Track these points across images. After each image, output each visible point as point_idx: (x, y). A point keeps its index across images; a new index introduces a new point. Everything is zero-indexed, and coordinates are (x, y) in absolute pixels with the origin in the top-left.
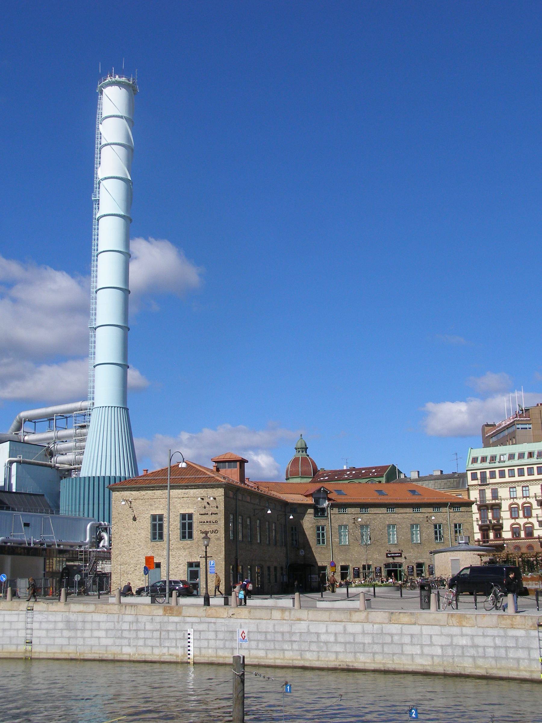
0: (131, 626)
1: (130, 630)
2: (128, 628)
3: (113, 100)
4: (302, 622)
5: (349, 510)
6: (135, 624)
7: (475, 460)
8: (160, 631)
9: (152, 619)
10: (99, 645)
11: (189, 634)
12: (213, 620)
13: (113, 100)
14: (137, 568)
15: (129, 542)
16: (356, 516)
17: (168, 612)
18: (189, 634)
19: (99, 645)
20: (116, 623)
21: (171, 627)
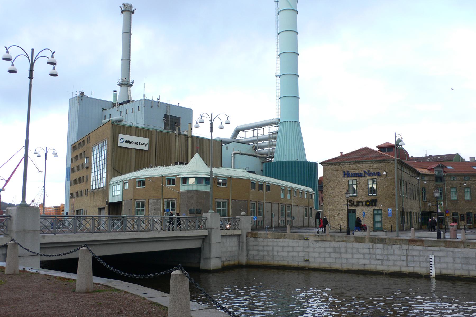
1: (382, 255)
11: (431, 259)
18: (431, 259)
20: (371, 250)
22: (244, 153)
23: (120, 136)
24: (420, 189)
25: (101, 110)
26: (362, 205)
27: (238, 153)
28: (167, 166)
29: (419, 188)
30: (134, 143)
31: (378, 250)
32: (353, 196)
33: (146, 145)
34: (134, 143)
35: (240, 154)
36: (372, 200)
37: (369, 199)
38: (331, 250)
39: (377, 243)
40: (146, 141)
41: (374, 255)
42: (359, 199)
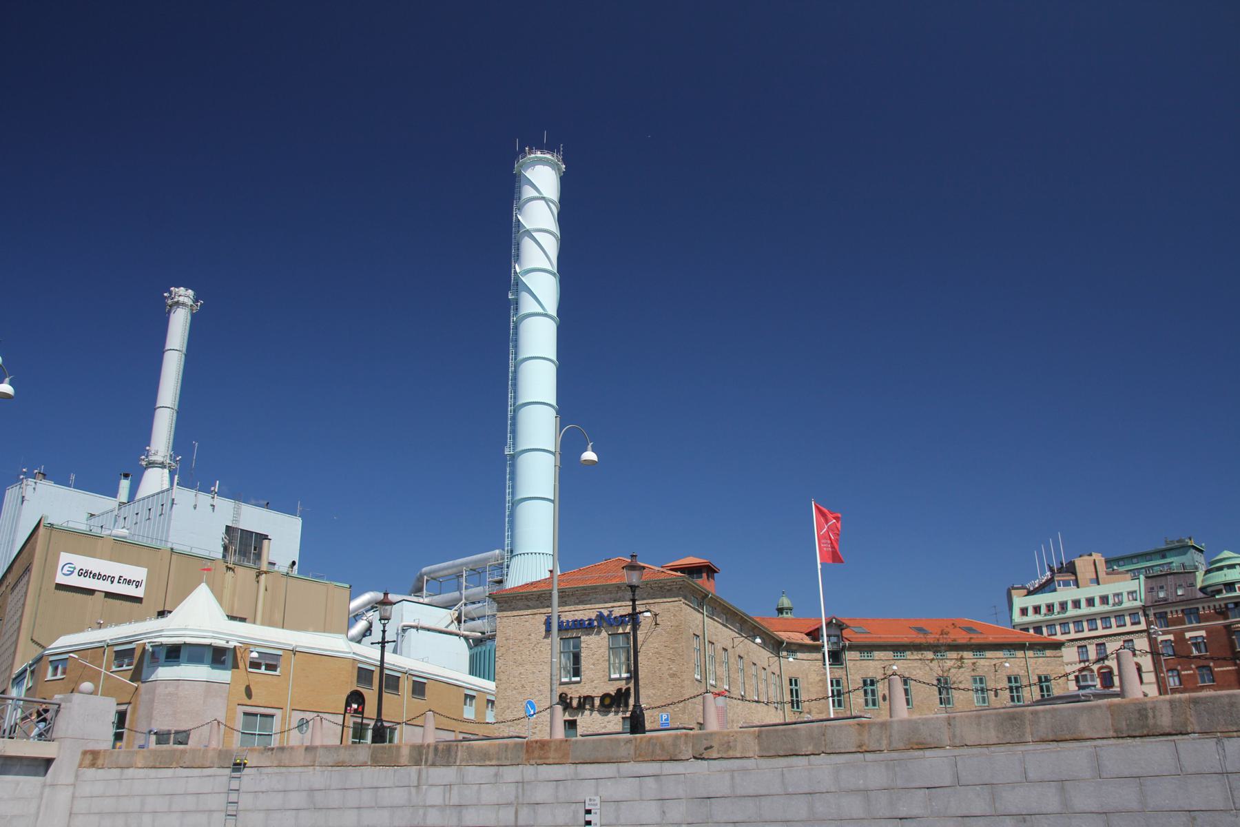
0: (447, 796)
1: (443, 808)
2: (439, 801)
3: (542, 179)
4: (928, 753)
5: (877, 654)
6: (455, 790)
7: (1024, 611)
8: (517, 805)
9: (496, 775)
10: (74, 785)
11: (588, 812)
12: (653, 768)
13: (542, 179)
14: (536, 731)
15: (523, 686)
16: (887, 663)
17: (536, 754)
18: (588, 812)
19: (74, 785)
20: (413, 790)
21: (542, 793)
22: (426, 625)
23: (65, 557)
24: (786, 683)
25: (86, 516)
26: (592, 709)
27: (412, 627)
28: (136, 621)
29: (780, 676)
30: (105, 578)
31: (434, 789)
32: (570, 683)
33: (138, 584)
34: (105, 578)
35: (417, 628)
36: (619, 690)
37: (612, 690)
38: (297, 799)
39: (433, 765)
40: (140, 573)
41: (421, 812)
42: (585, 691)
